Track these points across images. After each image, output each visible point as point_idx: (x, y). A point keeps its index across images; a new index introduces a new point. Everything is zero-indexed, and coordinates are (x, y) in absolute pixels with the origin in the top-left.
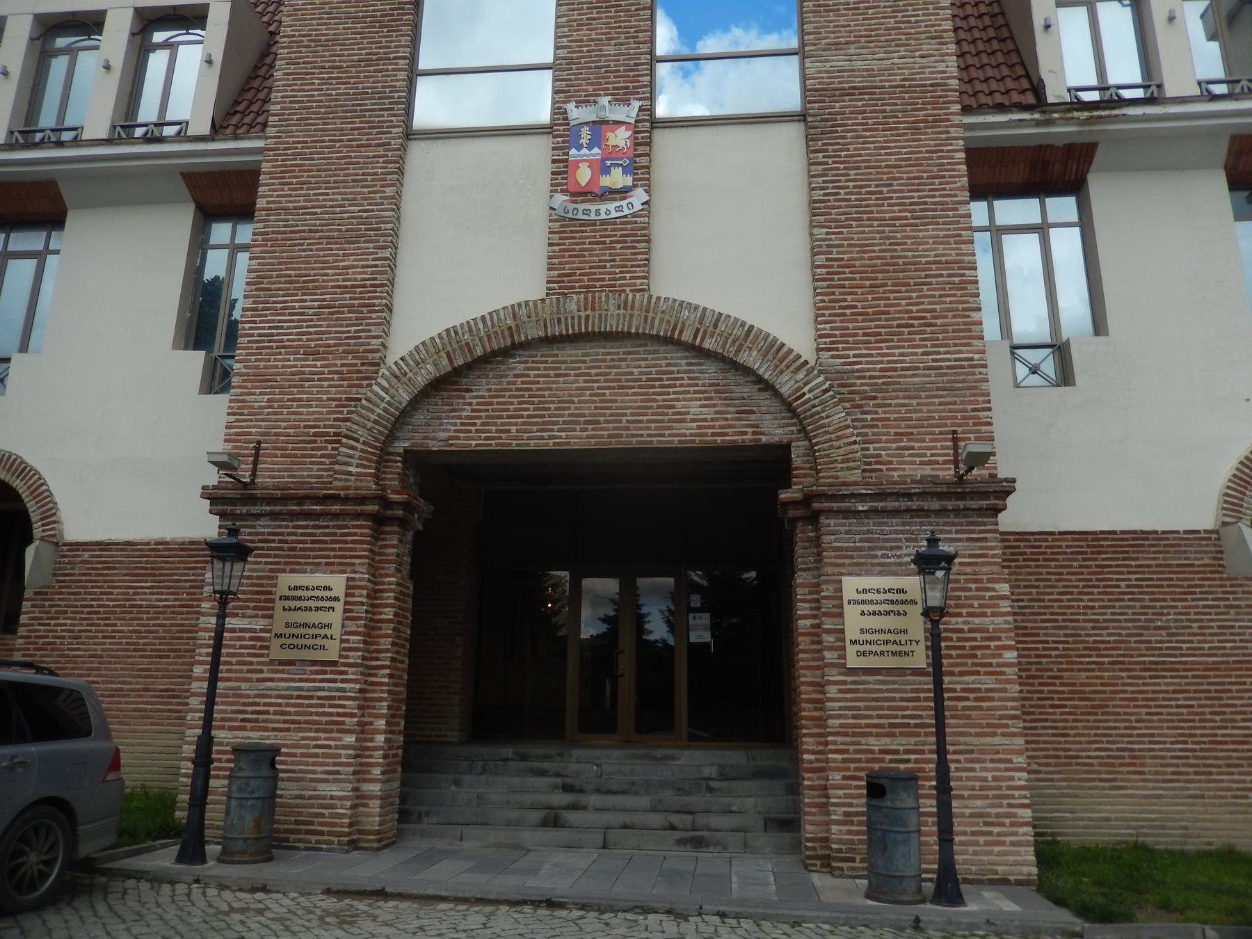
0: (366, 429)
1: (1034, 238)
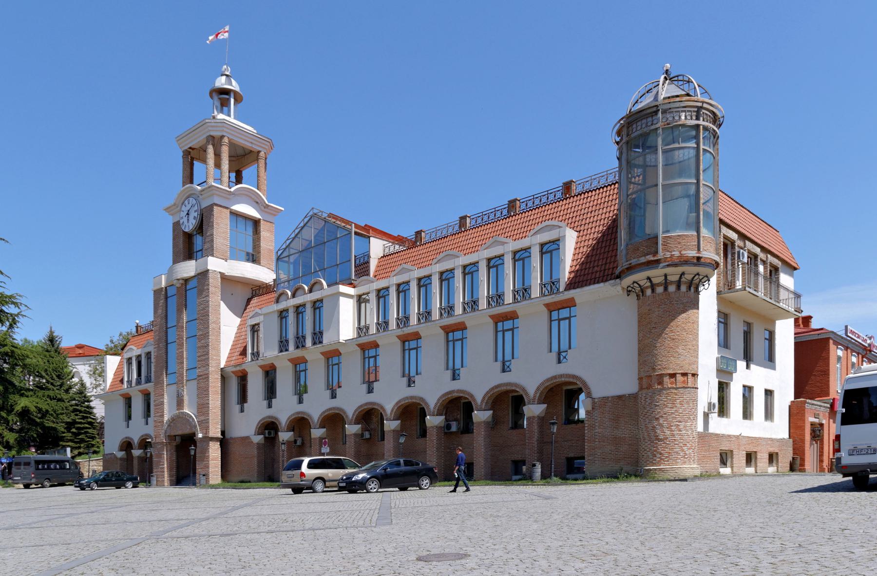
1: (506, 333)
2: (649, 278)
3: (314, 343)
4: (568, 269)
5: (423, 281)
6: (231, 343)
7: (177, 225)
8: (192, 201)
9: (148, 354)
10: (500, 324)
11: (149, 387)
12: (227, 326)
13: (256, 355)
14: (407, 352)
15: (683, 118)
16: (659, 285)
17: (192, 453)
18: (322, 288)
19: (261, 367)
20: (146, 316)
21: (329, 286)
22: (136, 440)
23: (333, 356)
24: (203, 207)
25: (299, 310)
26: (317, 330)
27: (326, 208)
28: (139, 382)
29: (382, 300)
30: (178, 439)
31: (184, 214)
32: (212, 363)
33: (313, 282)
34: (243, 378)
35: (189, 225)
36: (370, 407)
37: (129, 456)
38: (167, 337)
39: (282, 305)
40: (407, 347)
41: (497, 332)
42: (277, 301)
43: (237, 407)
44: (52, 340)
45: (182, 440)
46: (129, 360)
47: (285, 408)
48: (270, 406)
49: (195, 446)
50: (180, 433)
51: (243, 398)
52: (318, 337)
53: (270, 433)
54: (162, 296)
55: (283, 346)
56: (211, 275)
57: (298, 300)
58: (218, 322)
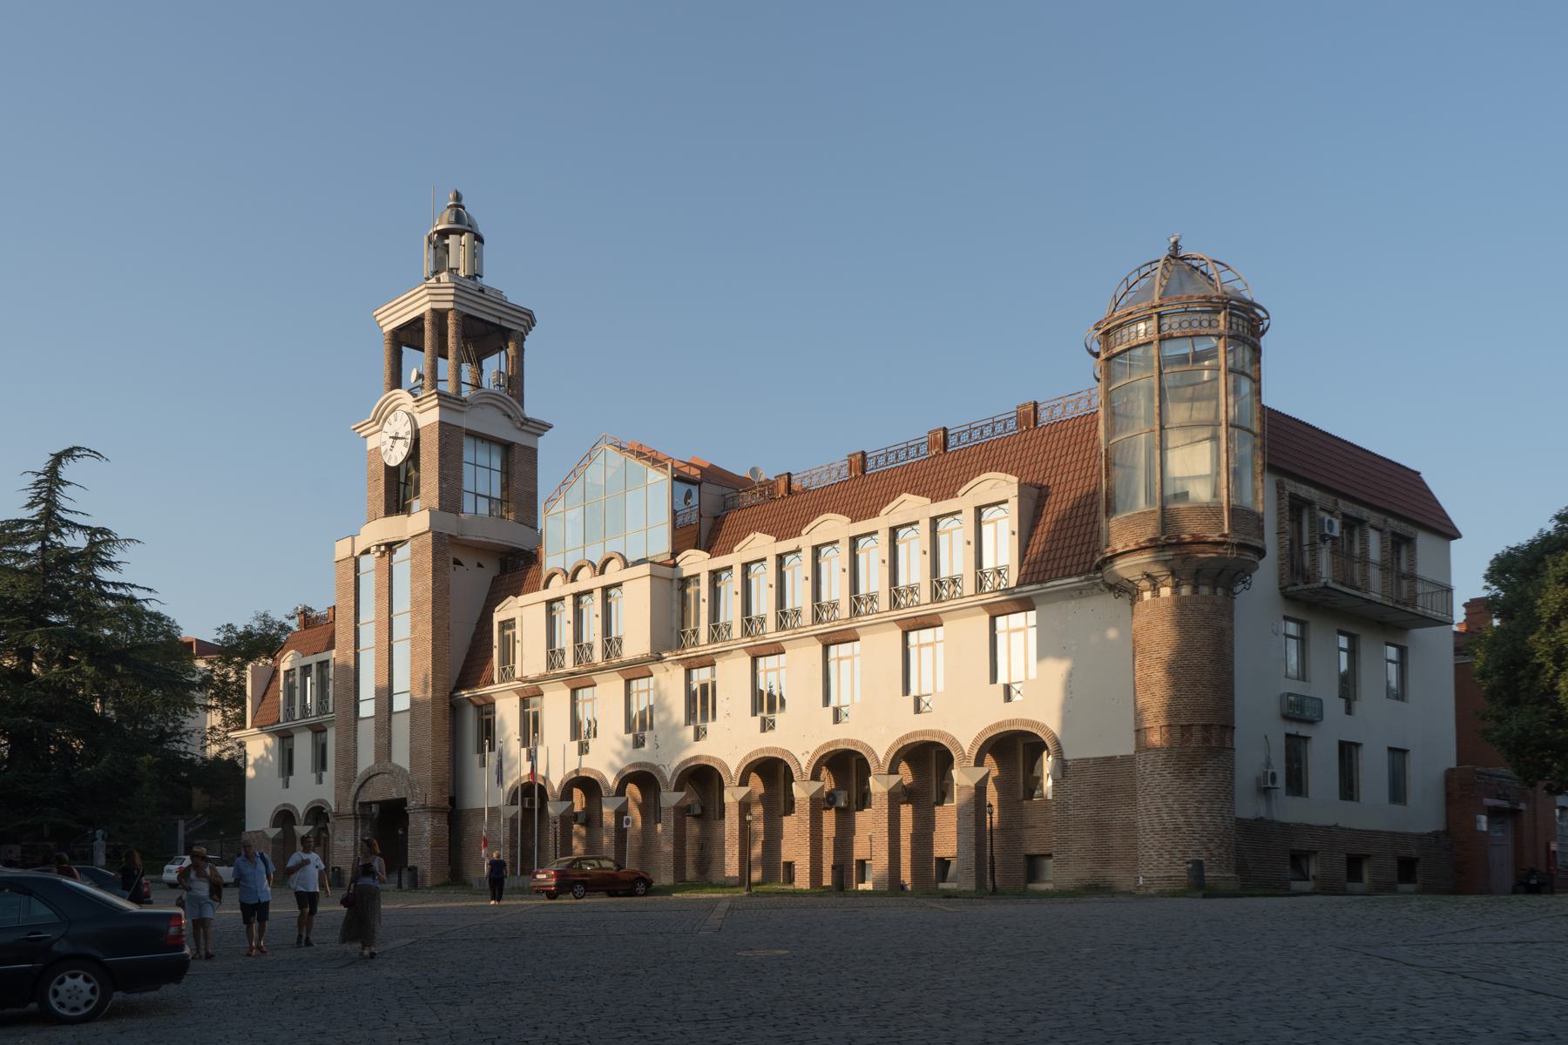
0: (351, 798)
22: (301, 809)
30: (375, 808)
45: (381, 811)
50: (380, 798)
57: (586, 580)
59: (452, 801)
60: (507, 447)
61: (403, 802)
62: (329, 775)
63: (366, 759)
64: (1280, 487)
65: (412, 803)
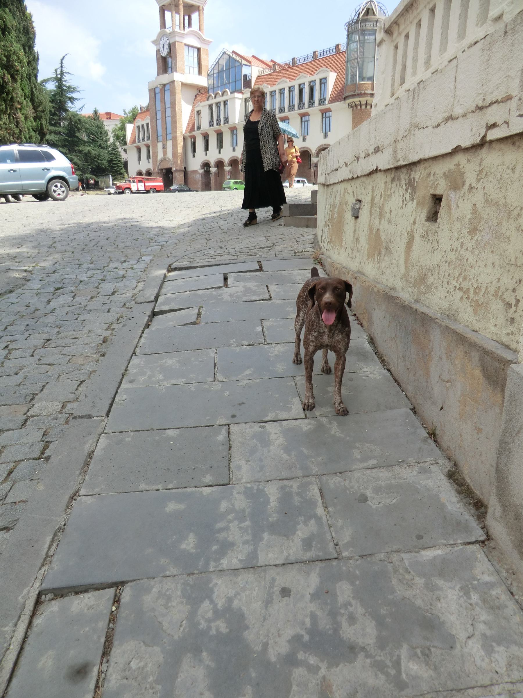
2: (360, 101)
3: (225, 123)
4: (330, 93)
5: (322, 81)
6: (188, 120)
7: (158, 51)
8: (165, 38)
9: (148, 124)
10: (324, 114)
11: (149, 142)
12: (185, 111)
13: (199, 127)
14: (324, 119)
15: (372, 25)
16: (363, 104)
17: (171, 178)
18: (228, 95)
19: (202, 134)
20: (144, 101)
21: (231, 93)
23: (233, 129)
24: (171, 42)
25: (218, 104)
26: (322, 97)
27: (230, 49)
28: (144, 140)
29: (323, 85)
30: (164, 171)
31: (161, 46)
32: (179, 132)
33: (224, 90)
34: (194, 139)
35: (164, 53)
36: (305, 149)
37: (207, 172)
38: (156, 116)
39: (210, 102)
40: (324, 116)
41: (323, 118)
42: (208, 100)
43: (192, 155)
44: (96, 112)
46: (138, 127)
47: (213, 156)
48: (220, 152)
49: (172, 174)
51: (194, 150)
52: (226, 120)
53: (207, 169)
54: (153, 92)
55: (211, 124)
56: (176, 84)
57: (218, 100)
58: (180, 110)
59: (185, 168)
60: (199, 50)
61: (171, 169)
62: (151, 160)
63: (160, 156)
64: (281, 426)
65: (174, 169)
